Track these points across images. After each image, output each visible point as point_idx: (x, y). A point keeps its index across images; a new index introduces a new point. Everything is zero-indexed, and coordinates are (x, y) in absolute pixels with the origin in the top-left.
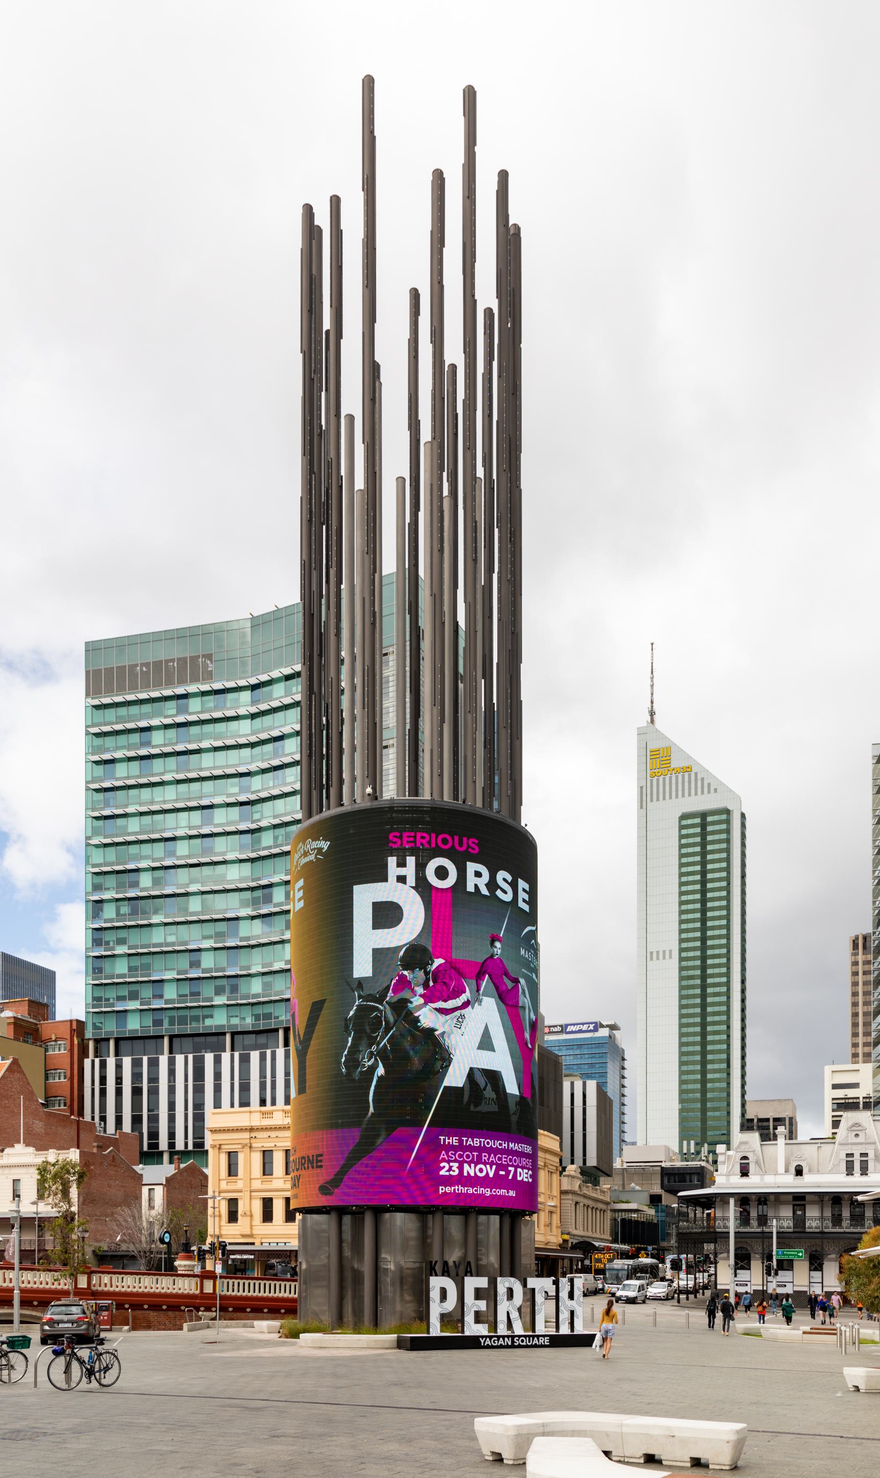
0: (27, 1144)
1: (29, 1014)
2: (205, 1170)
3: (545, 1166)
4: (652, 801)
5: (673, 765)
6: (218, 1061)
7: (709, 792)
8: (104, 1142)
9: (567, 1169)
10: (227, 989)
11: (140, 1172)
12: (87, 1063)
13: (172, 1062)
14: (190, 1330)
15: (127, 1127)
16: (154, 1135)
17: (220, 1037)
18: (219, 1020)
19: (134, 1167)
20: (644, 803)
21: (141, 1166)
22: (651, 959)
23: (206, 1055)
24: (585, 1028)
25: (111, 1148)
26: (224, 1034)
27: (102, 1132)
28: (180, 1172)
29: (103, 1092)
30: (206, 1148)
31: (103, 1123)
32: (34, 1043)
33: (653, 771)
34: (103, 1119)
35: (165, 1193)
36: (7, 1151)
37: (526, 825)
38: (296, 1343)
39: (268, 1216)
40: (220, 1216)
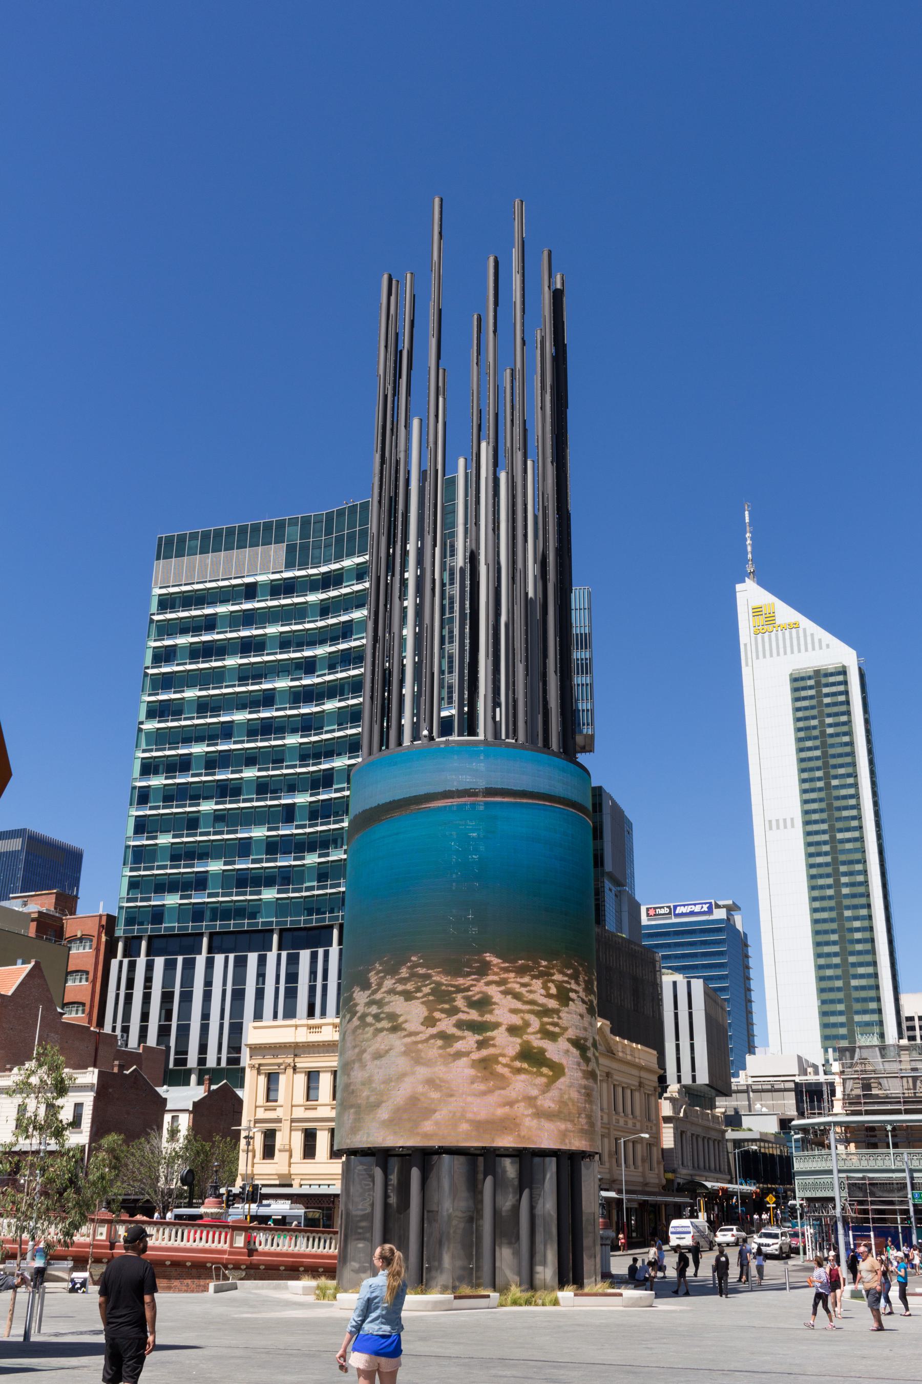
1: (55, 908)
2: (239, 1092)
3: (640, 1086)
4: (758, 658)
5: (778, 622)
6: (262, 961)
7: (821, 648)
8: (129, 1058)
9: (668, 1090)
11: (164, 1095)
12: (114, 963)
13: (210, 963)
14: (216, 1292)
15: (152, 1040)
16: (182, 1051)
17: (267, 934)
19: (157, 1089)
21: (165, 1087)
22: (771, 828)
24: (697, 909)
25: (135, 1067)
27: (124, 1045)
28: (211, 1093)
29: (129, 998)
30: (242, 1065)
31: (125, 1035)
32: (56, 941)
33: (757, 628)
34: (126, 1030)
35: (191, 1121)
38: (333, 1305)
39: (309, 1151)
40: (254, 1151)
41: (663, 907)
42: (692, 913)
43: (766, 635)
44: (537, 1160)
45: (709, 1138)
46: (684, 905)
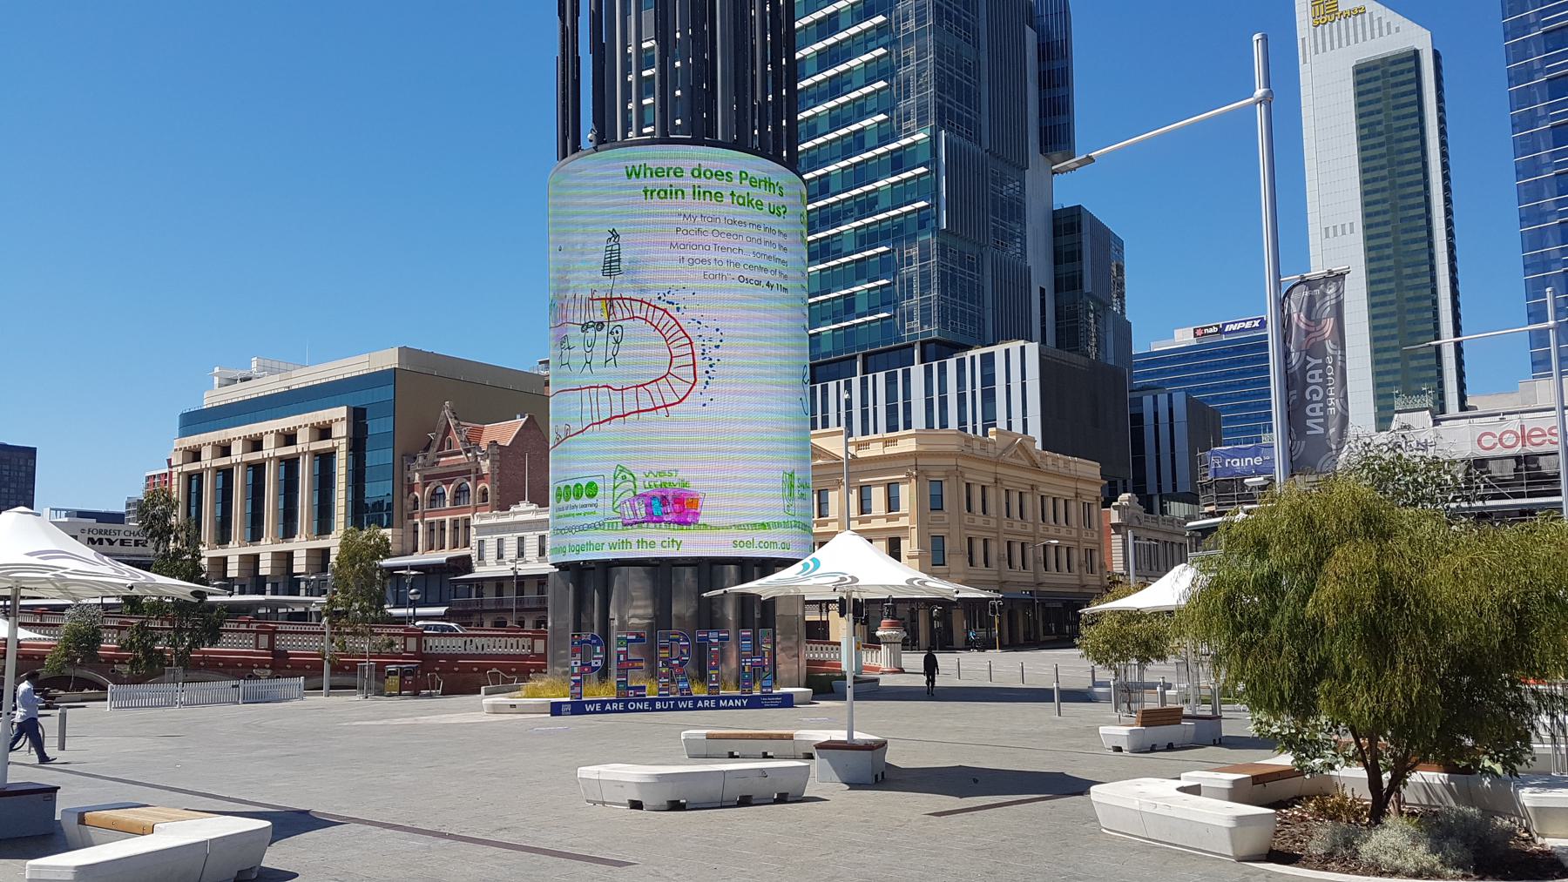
0: (532, 502)
4: (1316, 53)
20: (1308, 57)
23: (829, 383)
24: (1248, 325)
36: (513, 509)
41: (1211, 327)
42: (1242, 330)
43: (1327, 26)
44: (716, 568)
45: (1173, 543)
46: (1234, 323)
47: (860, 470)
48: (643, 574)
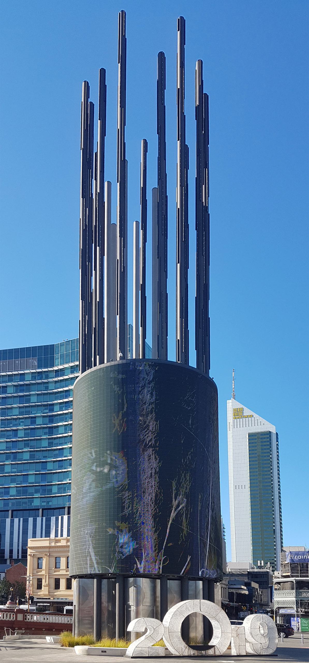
10: (41, 491)
13: (12, 522)
18: (36, 503)
26: (39, 509)
37: (213, 378)
47: (55, 550)
48: (149, 580)
